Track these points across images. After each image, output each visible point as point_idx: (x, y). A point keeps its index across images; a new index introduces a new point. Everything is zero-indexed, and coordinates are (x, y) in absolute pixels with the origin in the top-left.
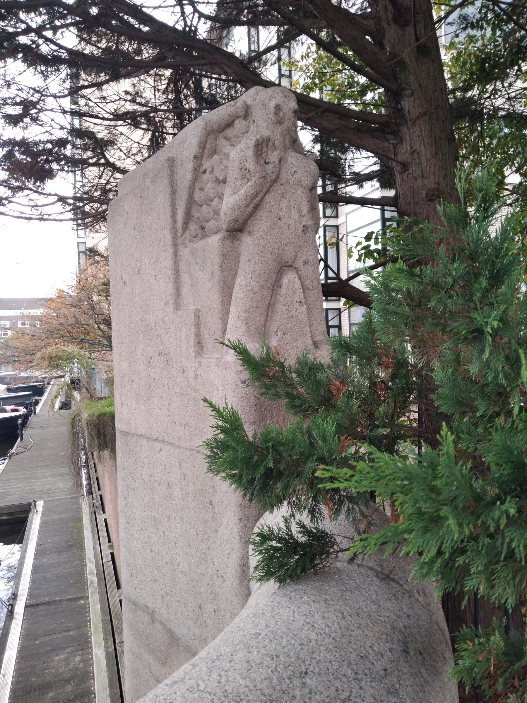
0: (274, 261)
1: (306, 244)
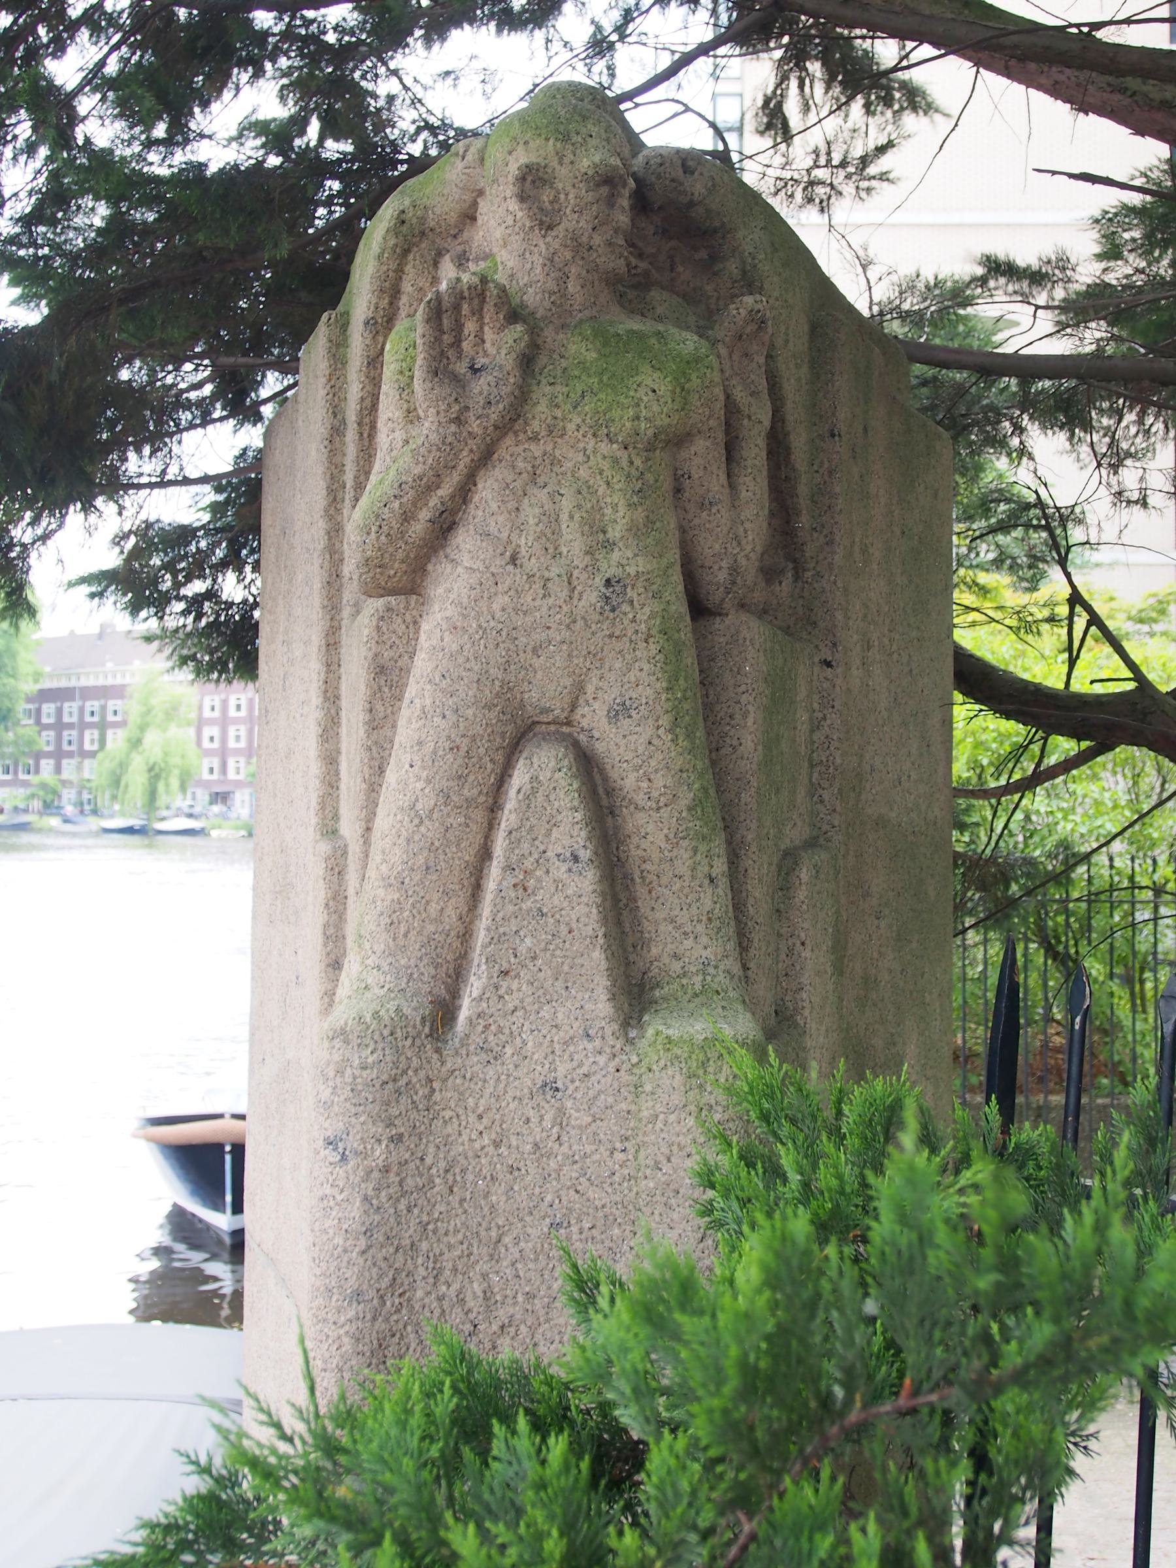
0: (489, 707)
1: (619, 646)
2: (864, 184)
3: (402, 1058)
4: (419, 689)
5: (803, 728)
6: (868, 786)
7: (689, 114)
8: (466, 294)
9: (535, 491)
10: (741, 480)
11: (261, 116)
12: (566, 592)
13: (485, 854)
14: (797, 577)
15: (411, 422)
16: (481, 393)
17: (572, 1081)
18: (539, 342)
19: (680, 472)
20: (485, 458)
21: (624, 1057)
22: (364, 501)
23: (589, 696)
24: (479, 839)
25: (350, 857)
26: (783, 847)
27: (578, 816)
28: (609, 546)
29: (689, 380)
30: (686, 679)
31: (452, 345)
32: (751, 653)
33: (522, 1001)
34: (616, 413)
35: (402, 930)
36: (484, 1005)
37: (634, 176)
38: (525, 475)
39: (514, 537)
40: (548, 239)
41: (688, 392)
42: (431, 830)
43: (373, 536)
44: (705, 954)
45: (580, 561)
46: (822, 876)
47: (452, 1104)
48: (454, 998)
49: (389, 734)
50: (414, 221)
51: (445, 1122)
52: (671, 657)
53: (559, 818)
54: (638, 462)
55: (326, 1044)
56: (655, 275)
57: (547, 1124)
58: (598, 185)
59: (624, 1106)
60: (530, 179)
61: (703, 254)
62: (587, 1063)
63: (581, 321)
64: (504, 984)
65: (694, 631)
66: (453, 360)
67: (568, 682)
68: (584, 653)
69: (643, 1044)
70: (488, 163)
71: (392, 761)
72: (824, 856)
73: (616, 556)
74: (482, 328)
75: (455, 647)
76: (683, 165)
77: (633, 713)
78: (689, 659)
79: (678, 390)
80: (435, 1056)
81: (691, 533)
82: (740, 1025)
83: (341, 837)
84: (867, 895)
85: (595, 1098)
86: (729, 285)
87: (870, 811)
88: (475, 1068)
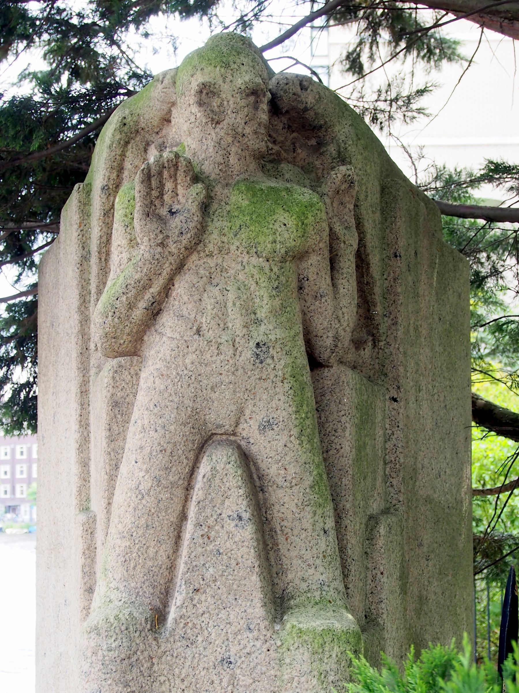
0: (185, 424)
1: (265, 385)
2: (409, 114)
3: (134, 644)
4: (141, 413)
5: (380, 440)
6: (420, 477)
7: (299, 65)
8: (166, 165)
9: (212, 288)
10: (340, 281)
11: (31, 70)
12: (231, 352)
13: (183, 517)
14: (374, 346)
15: (133, 247)
16: (176, 227)
17: (240, 657)
18: (212, 194)
19: (301, 277)
20: (180, 267)
21: (273, 642)
22: (104, 298)
23: (247, 417)
24: (179, 508)
25: (98, 522)
26: (368, 513)
27: (241, 492)
28: (258, 322)
29: (307, 218)
30: (307, 406)
31: (157, 197)
32: (347, 391)
33: (208, 608)
34: (261, 239)
35: (132, 564)
36: (185, 610)
37: (270, 90)
38: (205, 278)
39: (198, 317)
40: (217, 130)
41: (307, 225)
42: (149, 502)
43: (110, 318)
44: (321, 578)
45: (240, 331)
46: (393, 532)
47: (165, 672)
48: (165, 607)
49: (121, 444)
50: (132, 123)
51: (161, 684)
52: (298, 391)
53: (229, 493)
54: (275, 269)
55: (86, 636)
56: (284, 154)
57: (225, 684)
58: (247, 95)
59: (272, 672)
60: (205, 92)
61: (313, 142)
62: (249, 646)
63: (238, 182)
64: (197, 597)
65: (312, 377)
66: (158, 206)
67: (233, 408)
68: (244, 389)
69: (284, 634)
70: (178, 83)
71: (124, 460)
72: (394, 519)
73: (262, 328)
74: (176, 186)
75: (162, 387)
76: (301, 84)
77: (275, 427)
78: (309, 393)
79: (300, 224)
80: (154, 643)
81: (309, 315)
82: (346, 621)
83: (92, 511)
84: (420, 545)
85: (255, 668)
86: (330, 161)
87: (421, 493)
88: (179, 650)
